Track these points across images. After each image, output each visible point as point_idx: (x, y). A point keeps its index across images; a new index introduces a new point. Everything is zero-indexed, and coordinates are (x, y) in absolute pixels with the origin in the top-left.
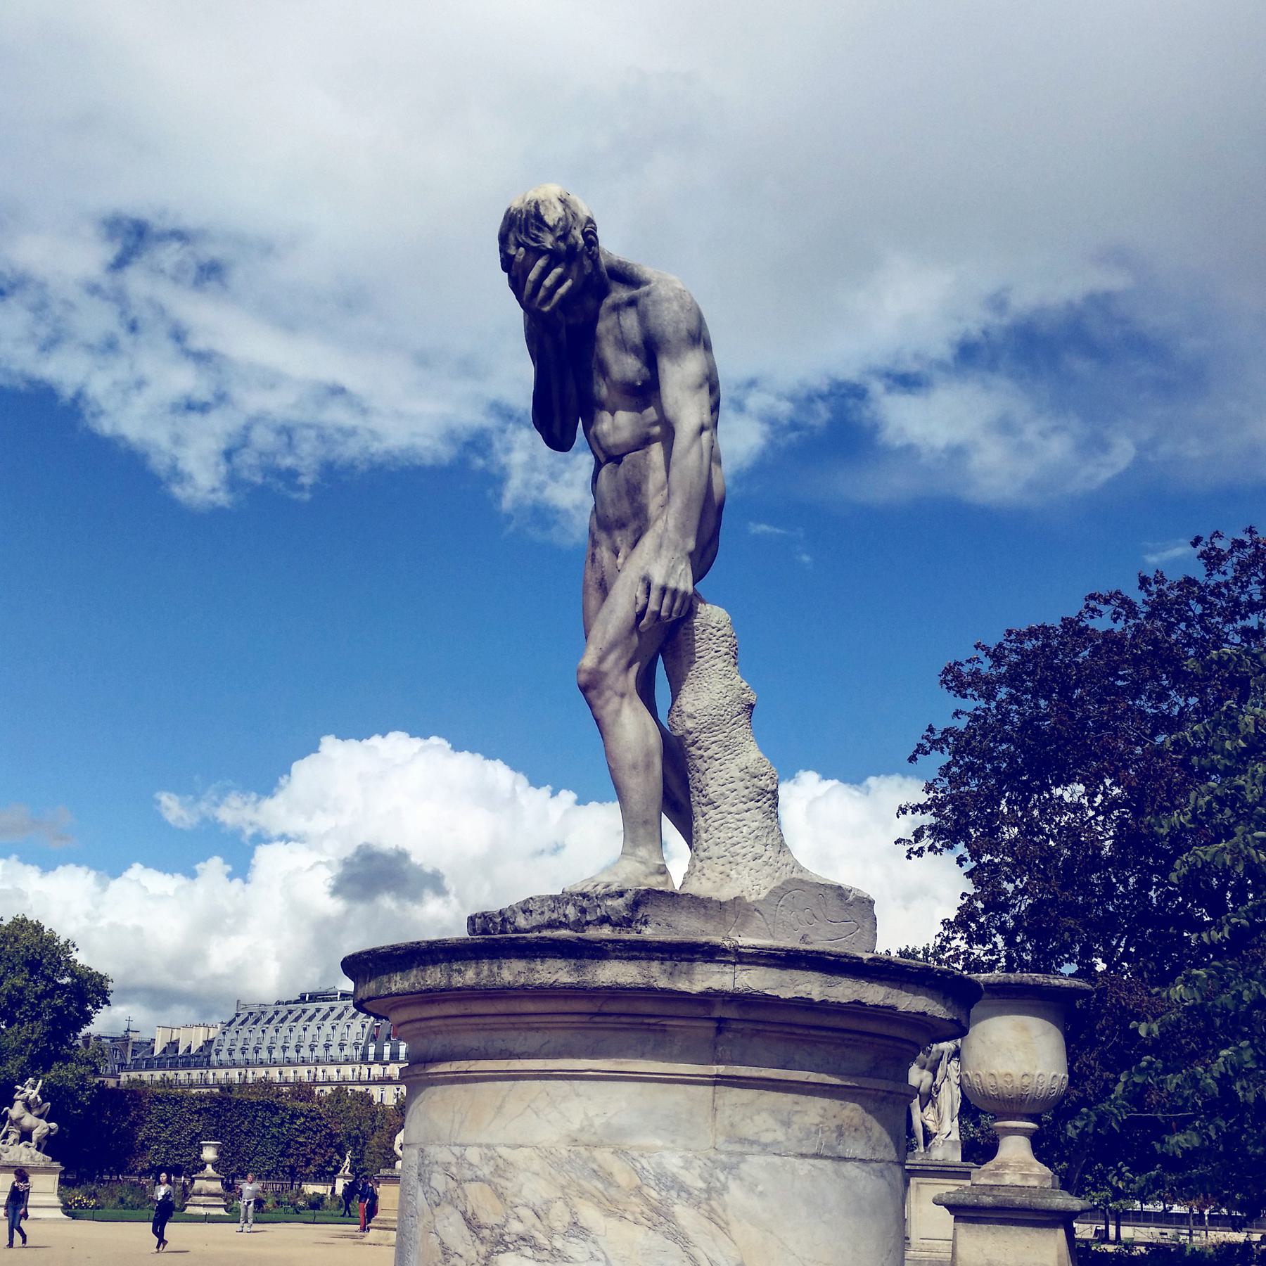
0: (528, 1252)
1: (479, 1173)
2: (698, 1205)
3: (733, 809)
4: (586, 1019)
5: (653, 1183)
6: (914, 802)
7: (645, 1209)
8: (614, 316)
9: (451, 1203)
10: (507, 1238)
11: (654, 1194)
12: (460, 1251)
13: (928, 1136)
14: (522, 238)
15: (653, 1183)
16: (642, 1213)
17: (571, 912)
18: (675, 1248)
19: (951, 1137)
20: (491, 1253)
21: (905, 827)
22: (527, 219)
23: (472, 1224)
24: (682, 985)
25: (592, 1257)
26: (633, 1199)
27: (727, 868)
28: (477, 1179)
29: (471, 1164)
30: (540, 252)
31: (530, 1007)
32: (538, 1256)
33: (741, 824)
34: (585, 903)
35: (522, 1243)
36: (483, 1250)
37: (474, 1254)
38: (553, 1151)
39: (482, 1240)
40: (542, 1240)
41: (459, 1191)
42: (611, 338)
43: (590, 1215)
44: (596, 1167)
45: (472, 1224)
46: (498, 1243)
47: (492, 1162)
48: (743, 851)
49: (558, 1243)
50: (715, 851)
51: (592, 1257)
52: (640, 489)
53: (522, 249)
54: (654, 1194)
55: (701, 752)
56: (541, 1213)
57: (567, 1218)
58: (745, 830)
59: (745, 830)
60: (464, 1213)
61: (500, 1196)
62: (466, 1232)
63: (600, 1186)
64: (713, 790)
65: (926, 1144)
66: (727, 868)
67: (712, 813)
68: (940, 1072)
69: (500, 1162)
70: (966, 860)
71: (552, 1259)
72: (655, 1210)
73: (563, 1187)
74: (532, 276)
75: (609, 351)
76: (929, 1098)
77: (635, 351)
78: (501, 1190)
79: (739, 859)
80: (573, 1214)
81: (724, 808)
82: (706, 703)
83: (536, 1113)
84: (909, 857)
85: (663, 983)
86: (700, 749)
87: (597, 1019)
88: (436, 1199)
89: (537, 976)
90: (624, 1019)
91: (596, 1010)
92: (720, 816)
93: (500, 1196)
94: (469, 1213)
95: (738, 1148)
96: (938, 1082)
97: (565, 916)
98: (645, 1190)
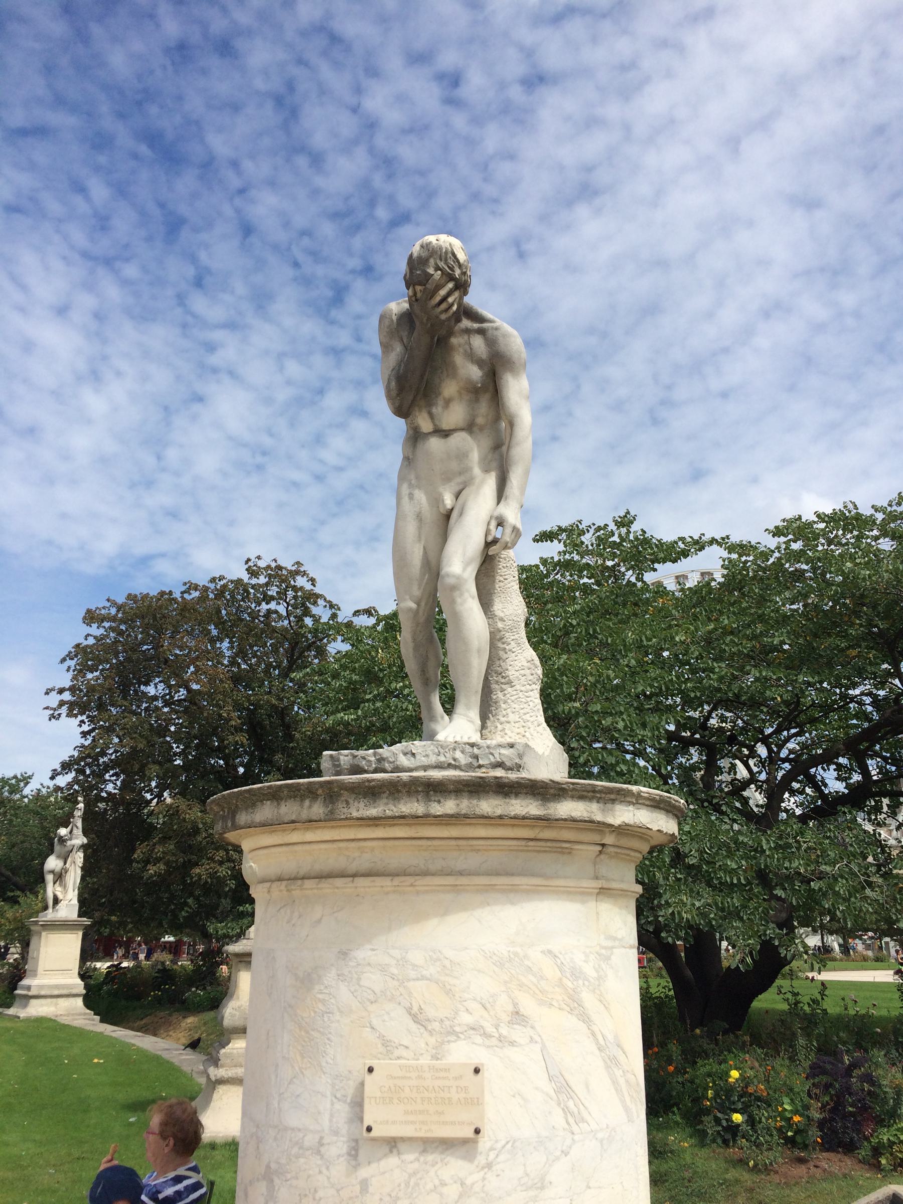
0: (479, 1039)
1: (424, 972)
2: (594, 991)
3: (523, 689)
4: (523, 843)
5: (568, 976)
6: (59, 685)
7: (566, 998)
8: (466, 337)
9: (392, 999)
10: (457, 1029)
11: (569, 984)
12: (405, 1043)
13: (56, 901)
14: (441, 264)
15: (568, 976)
16: (564, 1000)
17: (463, 759)
18: (582, 1026)
19: (72, 902)
20: (443, 1043)
21: (54, 699)
22: (446, 253)
23: (417, 1017)
24: (610, 820)
25: (532, 1040)
26: (557, 989)
27: (522, 730)
28: (423, 978)
29: (414, 966)
30: (451, 278)
31: (482, 832)
32: (487, 1042)
33: (529, 699)
34: (476, 751)
35: (472, 1032)
36: (432, 1041)
37: (423, 1045)
38: (496, 952)
39: (431, 1033)
40: (490, 1029)
41: (401, 989)
42: (461, 350)
43: (528, 1005)
44: (531, 965)
45: (417, 1017)
46: (449, 1033)
47: (438, 963)
48: (532, 719)
49: (504, 1031)
50: (512, 717)
51: (532, 1040)
52: (467, 456)
53: (439, 272)
54: (569, 984)
55: (505, 646)
56: (488, 1005)
57: (510, 1008)
58: (531, 703)
59: (531, 703)
60: (409, 1011)
61: (449, 992)
62: (414, 1027)
63: (534, 980)
64: (512, 673)
65: (54, 908)
66: (522, 730)
67: (510, 690)
68: (69, 860)
69: (447, 963)
70: (84, 723)
71: (500, 1044)
72: (571, 997)
73: (506, 982)
74: (443, 292)
75: (459, 359)
76: (59, 877)
77: (480, 363)
78: (448, 987)
79: (529, 724)
80: (515, 1005)
81: (518, 687)
82: (511, 612)
83: (480, 921)
84: (50, 720)
85: (599, 817)
86: (503, 643)
87: (531, 843)
88: (371, 997)
89: (511, 808)
90: (549, 844)
91: (532, 836)
92: (515, 693)
93: (449, 992)
94: (415, 1009)
95: (609, 943)
96: (67, 865)
97: (455, 760)
98: (565, 981)
